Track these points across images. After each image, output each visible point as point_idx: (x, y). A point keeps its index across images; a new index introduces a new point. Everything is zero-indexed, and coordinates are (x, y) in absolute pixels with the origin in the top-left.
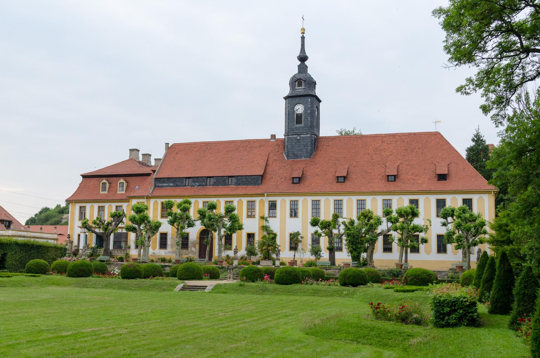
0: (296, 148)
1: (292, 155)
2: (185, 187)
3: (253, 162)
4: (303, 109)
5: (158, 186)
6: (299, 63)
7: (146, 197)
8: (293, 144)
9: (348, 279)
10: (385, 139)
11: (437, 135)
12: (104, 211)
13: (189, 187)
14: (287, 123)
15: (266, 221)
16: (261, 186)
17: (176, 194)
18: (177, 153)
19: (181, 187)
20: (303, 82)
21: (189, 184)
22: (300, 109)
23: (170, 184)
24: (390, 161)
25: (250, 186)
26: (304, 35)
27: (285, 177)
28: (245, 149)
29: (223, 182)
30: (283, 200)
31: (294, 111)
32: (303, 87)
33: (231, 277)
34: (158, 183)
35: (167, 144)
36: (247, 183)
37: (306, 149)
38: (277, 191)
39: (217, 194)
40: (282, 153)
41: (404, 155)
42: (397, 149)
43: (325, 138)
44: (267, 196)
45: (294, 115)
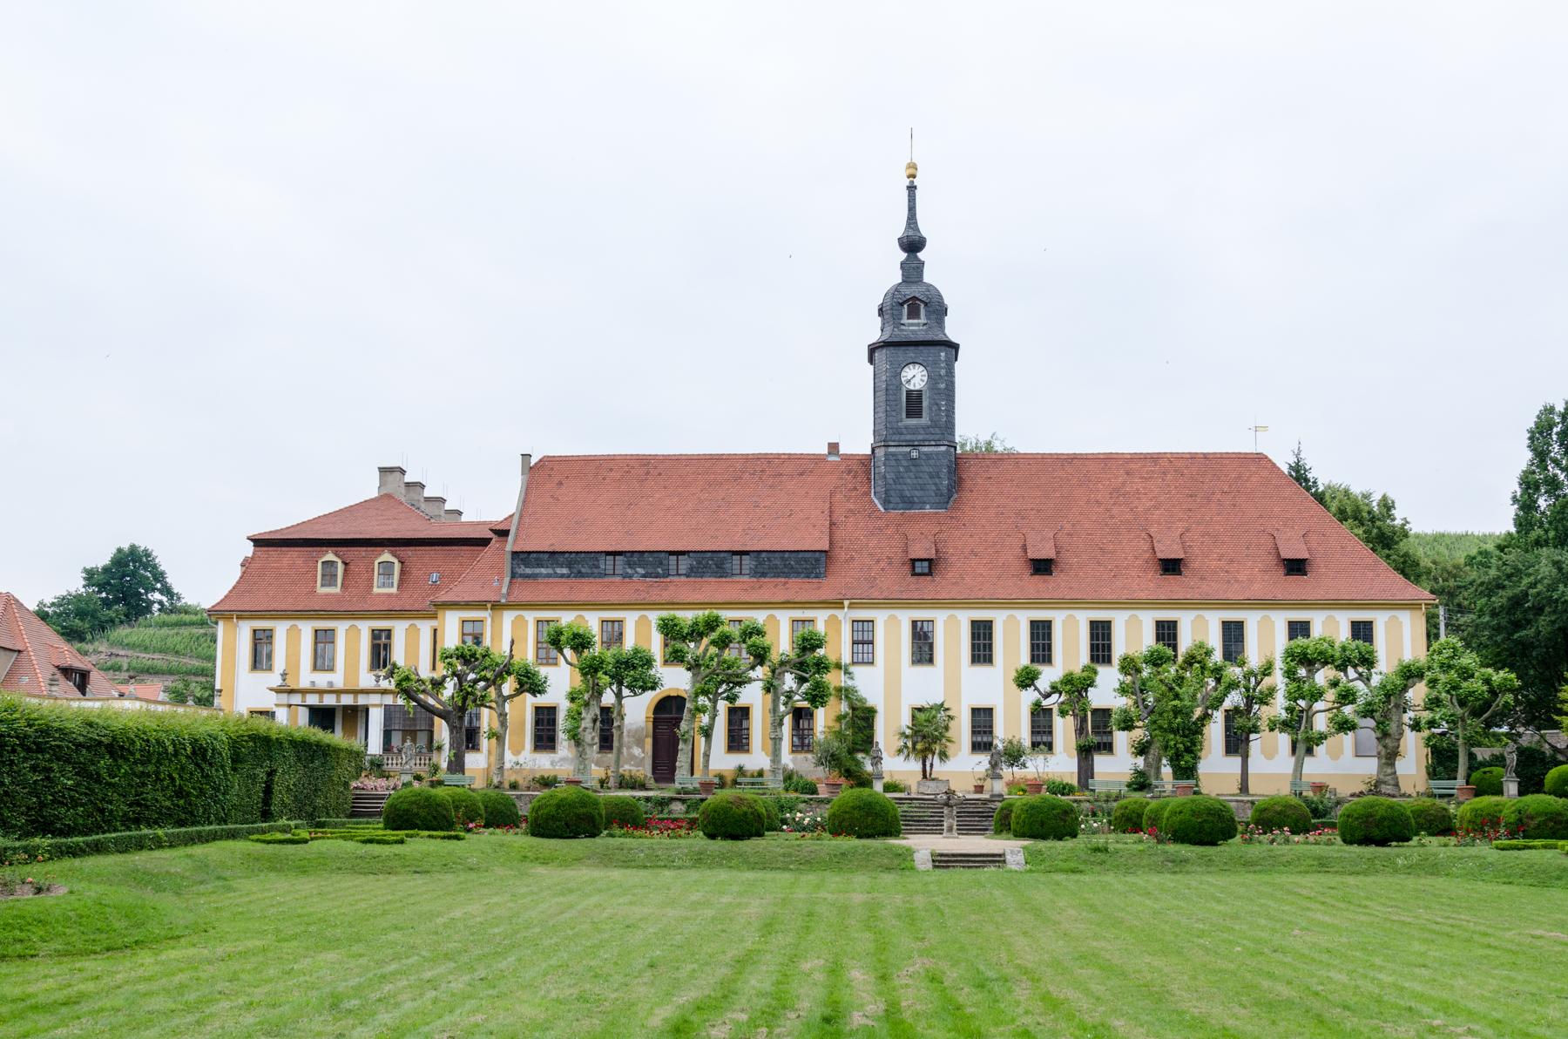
0: (909, 481)
1: (898, 500)
2: (606, 579)
4: (926, 379)
5: (522, 576)
6: (904, 256)
9: (1377, 826)
10: (1132, 466)
12: (333, 642)
13: (618, 579)
14: (882, 415)
15: (845, 673)
16: (824, 581)
17: (582, 597)
18: (560, 483)
19: (591, 580)
20: (922, 306)
21: (617, 572)
22: (915, 377)
23: (559, 571)
24: (1159, 523)
25: (794, 580)
27: (888, 558)
29: (718, 567)
30: (893, 617)
31: (901, 383)
32: (923, 320)
33: (955, 827)
34: (522, 567)
35: (526, 457)
36: (786, 570)
37: (935, 484)
38: (876, 595)
39: (706, 601)
40: (868, 494)
41: (1190, 510)
42: (1169, 492)
44: (849, 608)
45: (901, 394)
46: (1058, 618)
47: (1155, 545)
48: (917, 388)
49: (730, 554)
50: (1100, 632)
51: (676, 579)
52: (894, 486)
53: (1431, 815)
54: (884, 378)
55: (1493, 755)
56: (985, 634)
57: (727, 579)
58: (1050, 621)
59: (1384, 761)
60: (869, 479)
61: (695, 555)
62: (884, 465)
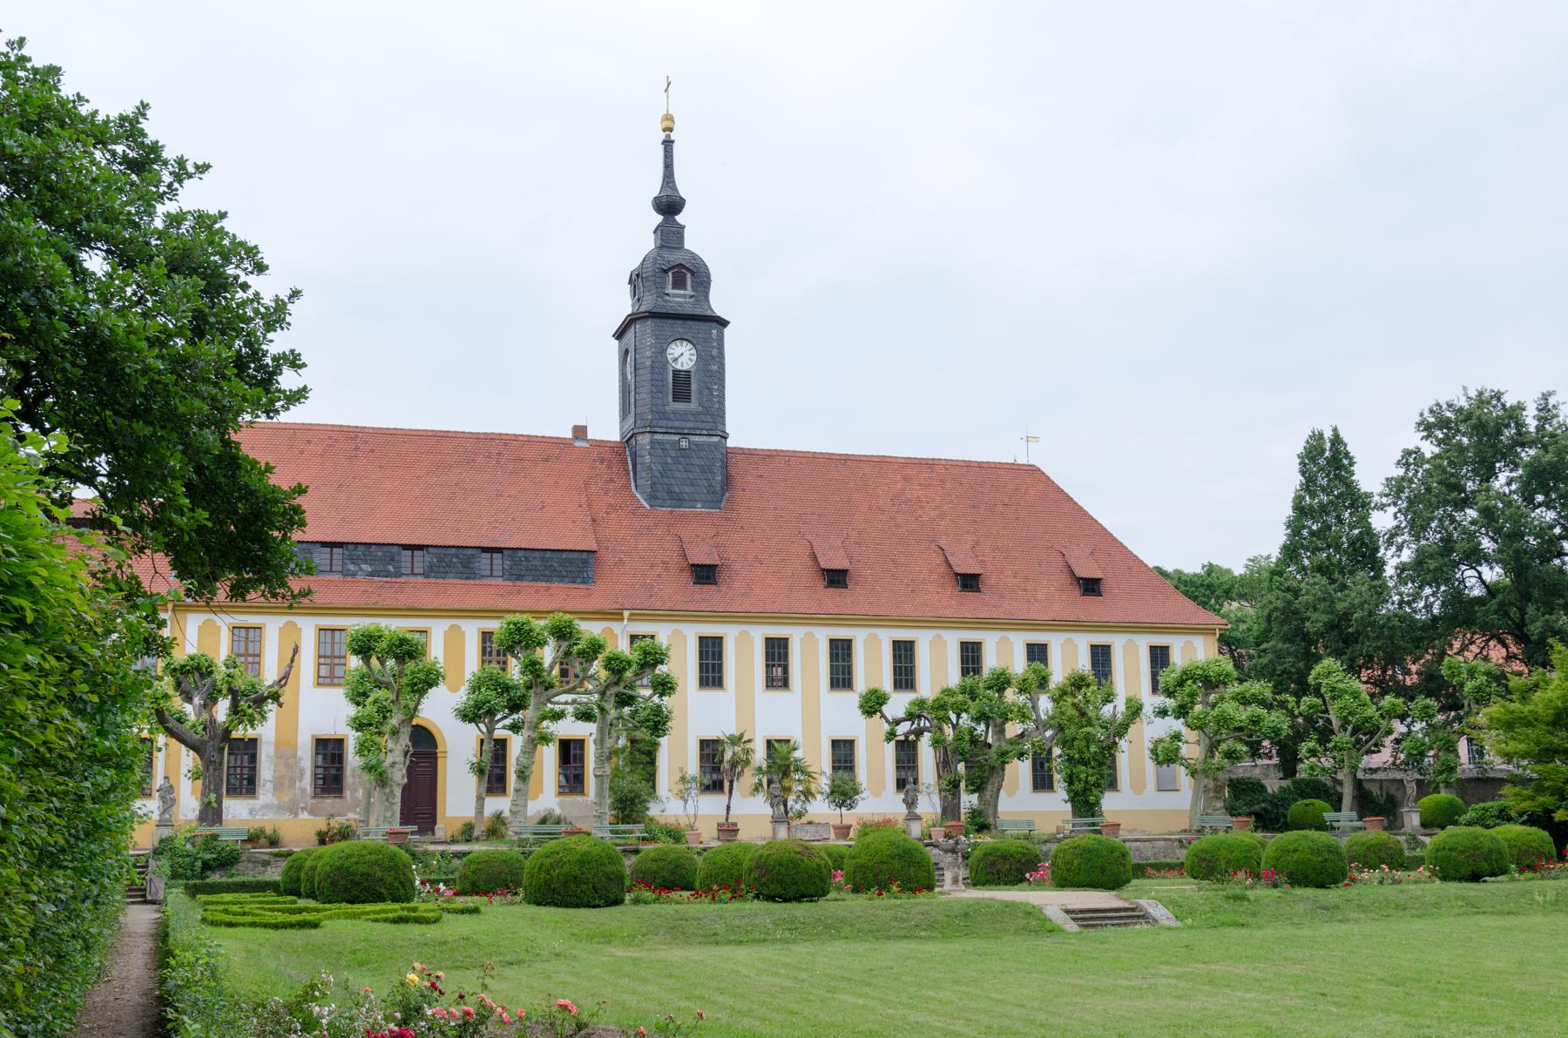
0: (677, 474)
3: (543, 507)
4: (694, 358)
6: (659, 218)
7: (175, 606)
8: (669, 460)
9: (1486, 860)
10: (909, 471)
11: (1033, 471)
13: (337, 577)
21: (334, 568)
22: (683, 356)
25: (556, 584)
26: (672, 134)
28: (498, 462)
30: (1189, 642)
36: (547, 573)
37: (707, 480)
38: (658, 605)
39: (451, 607)
43: (742, 451)
44: (629, 620)
45: (667, 374)
46: (860, 638)
47: (950, 558)
48: (686, 368)
49: (480, 550)
50: (710, 649)
51: (412, 579)
52: (660, 480)
53: (1391, 848)
54: (648, 353)
55: (1281, 787)
56: (713, 653)
57: (477, 582)
58: (787, 639)
59: (1212, 794)
60: (627, 470)
61: (436, 550)
62: (650, 454)
